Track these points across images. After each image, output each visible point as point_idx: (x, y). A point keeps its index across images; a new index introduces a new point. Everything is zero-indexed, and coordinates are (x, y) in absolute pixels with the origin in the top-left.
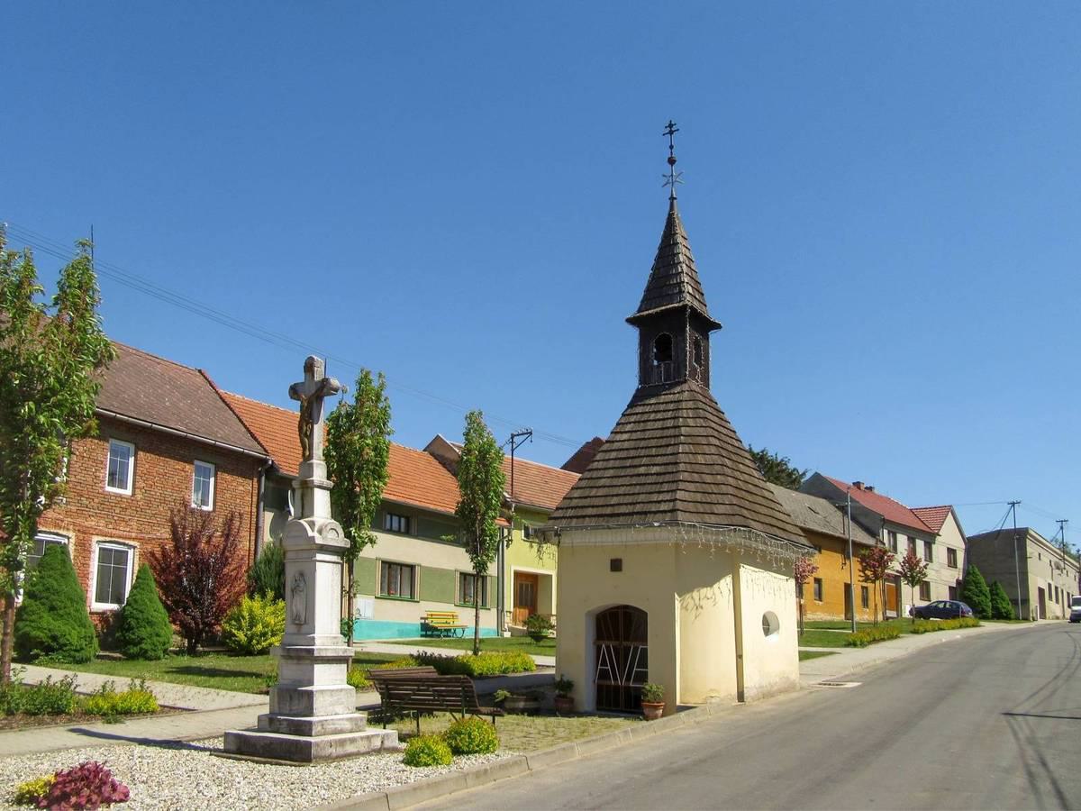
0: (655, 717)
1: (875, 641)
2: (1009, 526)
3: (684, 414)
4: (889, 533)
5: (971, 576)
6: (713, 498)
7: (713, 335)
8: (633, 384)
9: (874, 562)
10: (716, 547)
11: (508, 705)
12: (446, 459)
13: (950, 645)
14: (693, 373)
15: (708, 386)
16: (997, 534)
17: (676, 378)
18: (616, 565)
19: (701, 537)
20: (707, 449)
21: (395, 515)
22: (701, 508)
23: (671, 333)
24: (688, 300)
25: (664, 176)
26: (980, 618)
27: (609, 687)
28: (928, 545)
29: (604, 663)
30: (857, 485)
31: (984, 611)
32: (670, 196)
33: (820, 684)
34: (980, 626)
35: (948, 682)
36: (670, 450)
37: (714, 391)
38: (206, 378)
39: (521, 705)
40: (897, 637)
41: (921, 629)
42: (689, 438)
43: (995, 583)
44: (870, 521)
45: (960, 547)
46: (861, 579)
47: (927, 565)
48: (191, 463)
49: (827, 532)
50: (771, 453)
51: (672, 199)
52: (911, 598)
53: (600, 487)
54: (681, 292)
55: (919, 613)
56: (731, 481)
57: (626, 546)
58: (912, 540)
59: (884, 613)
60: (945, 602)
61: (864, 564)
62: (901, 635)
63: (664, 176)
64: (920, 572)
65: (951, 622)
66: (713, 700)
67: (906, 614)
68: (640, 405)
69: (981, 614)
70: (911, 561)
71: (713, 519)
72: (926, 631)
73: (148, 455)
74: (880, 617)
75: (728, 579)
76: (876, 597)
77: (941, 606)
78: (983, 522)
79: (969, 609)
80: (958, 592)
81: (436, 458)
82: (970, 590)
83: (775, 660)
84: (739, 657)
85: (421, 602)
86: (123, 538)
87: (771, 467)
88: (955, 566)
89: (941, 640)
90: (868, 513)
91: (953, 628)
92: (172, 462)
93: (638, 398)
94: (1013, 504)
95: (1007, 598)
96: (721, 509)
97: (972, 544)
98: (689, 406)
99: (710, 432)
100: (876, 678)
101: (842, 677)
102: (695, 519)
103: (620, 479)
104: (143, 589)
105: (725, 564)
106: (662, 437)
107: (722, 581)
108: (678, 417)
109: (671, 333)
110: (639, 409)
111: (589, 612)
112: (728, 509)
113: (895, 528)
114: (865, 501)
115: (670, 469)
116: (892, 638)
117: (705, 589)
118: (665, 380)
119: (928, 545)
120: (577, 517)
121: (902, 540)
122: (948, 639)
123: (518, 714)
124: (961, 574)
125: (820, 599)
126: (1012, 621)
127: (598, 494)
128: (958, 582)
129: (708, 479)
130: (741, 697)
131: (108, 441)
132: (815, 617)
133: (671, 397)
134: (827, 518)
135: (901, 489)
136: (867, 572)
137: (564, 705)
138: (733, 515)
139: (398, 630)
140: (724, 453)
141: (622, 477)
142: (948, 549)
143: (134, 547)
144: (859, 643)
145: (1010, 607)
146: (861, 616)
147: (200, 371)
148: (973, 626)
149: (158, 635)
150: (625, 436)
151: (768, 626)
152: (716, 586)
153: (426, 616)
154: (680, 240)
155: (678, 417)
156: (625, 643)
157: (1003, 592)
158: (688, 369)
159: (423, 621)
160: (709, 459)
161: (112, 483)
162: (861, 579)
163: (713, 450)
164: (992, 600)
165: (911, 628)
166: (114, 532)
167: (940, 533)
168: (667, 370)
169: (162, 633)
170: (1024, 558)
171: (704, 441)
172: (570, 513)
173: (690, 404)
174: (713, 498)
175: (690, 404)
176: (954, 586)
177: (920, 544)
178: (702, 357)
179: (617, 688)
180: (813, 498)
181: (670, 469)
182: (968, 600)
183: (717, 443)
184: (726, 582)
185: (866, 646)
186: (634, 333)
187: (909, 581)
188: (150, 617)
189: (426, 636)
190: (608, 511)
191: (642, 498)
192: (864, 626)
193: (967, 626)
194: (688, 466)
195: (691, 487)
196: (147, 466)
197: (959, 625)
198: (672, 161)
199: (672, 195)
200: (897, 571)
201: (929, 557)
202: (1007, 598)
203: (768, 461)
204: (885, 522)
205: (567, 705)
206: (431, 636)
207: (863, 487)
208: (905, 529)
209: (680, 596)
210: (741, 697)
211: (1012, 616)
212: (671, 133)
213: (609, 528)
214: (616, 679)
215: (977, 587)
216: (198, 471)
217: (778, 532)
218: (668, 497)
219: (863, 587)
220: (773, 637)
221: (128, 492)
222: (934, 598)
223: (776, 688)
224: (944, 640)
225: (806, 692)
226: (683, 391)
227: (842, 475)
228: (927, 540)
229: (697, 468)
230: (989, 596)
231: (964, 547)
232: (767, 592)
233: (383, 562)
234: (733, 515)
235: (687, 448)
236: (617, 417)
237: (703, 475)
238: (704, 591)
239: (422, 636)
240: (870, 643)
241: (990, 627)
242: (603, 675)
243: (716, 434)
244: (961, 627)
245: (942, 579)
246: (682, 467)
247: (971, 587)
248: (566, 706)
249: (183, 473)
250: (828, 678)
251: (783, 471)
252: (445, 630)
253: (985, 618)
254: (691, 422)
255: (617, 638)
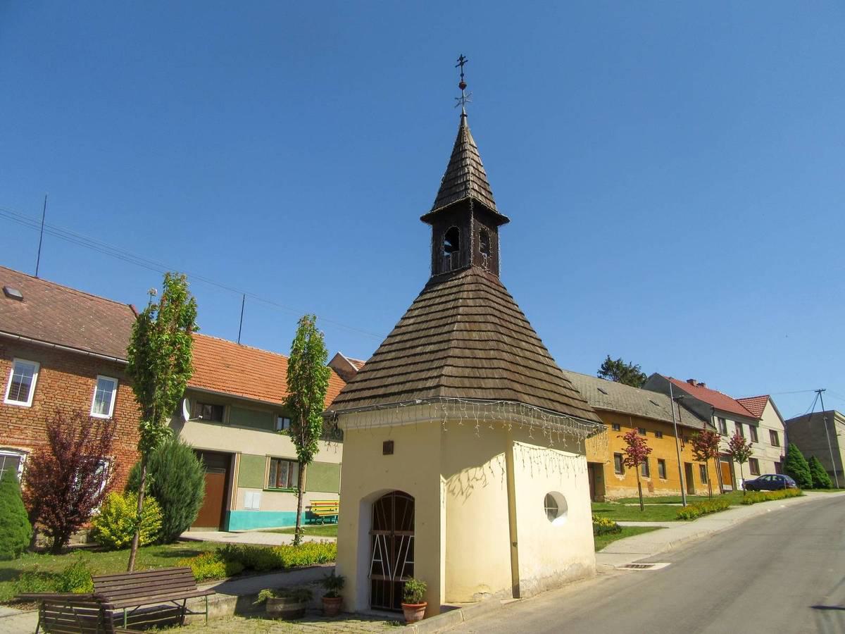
0: (416, 620)
1: (704, 513)
2: (818, 409)
3: (465, 295)
4: (719, 420)
5: (791, 453)
6: (483, 373)
7: (502, 229)
8: (427, 275)
9: (705, 444)
10: (481, 422)
11: (269, 608)
12: (343, 371)
13: (776, 514)
14: (479, 260)
15: (497, 273)
16: (810, 417)
17: (461, 265)
18: (388, 448)
19: (463, 413)
20: (483, 327)
21: (287, 418)
22: (467, 382)
23: (461, 225)
24: (472, 194)
25: (456, 98)
26: (803, 489)
27: (381, 581)
28: (753, 429)
29: (377, 556)
30: (691, 382)
31: (806, 482)
32: (461, 114)
33: (627, 566)
34: (729, 509)
35: (757, 562)
36: (446, 329)
37: (504, 277)
38: (134, 311)
39: (280, 607)
40: (727, 509)
41: (750, 500)
42: (465, 317)
43: (813, 458)
44: (704, 410)
45: (780, 429)
46: (695, 458)
47: (751, 444)
48: (94, 377)
49: (666, 420)
50: (626, 363)
51: (463, 115)
52: (743, 472)
53: (381, 369)
54: (467, 189)
55: (749, 486)
56: (505, 356)
57: (392, 427)
58: (739, 425)
59: (721, 487)
60: (772, 476)
61: (696, 445)
62: (731, 507)
63: (456, 98)
64: (746, 451)
65: (777, 493)
66: (483, 597)
67: (740, 488)
68: (429, 292)
69: (803, 485)
70: (738, 442)
71: (480, 394)
72: (754, 502)
73: (51, 371)
74: (716, 491)
75: (501, 458)
76: (713, 474)
77: (769, 479)
78: (797, 408)
79: (792, 481)
80: (783, 466)
81: (335, 372)
82: (792, 465)
83: (561, 546)
84: (514, 544)
85: (307, 492)
86: (16, 445)
87: (626, 373)
88: (778, 445)
89: (766, 510)
90: (700, 403)
91: (779, 499)
92: (74, 377)
93: (430, 286)
94: (820, 391)
95: (824, 470)
96: (490, 383)
97: (790, 426)
98: (470, 289)
99: (490, 311)
100: (683, 558)
101: (658, 555)
102: (458, 394)
103: (399, 360)
104: (5, 491)
105: (497, 441)
106: (442, 318)
107: (494, 460)
108: (459, 299)
109: (461, 225)
110: (428, 296)
111: (363, 498)
112: (498, 383)
113: (724, 415)
114: (695, 393)
115: (443, 346)
116: (721, 509)
117: (474, 469)
118: (453, 268)
119: (753, 429)
120: (354, 400)
121: (731, 425)
122: (773, 509)
123: (276, 619)
124: (784, 451)
125: (665, 478)
126: (831, 490)
127: (377, 376)
128: (782, 458)
129: (480, 354)
130: (516, 592)
131: (12, 361)
132: (662, 493)
133: (456, 282)
134: (660, 407)
135: (727, 384)
136: (699, 452)
137: (330, 606)
138: (502, 389)
139: (284, 519)
140: (502, 330)
141: (402, 357)
142: (770, 430)
143: (27, 453)
144: (688, 516)
145: (827, 478)
146: (701, 490)
147: (130, 306)
148: (797, 496)
149: (11, 535)
150: (412, 321)
151: (553, 506)
152: (486, 466)
153: (310, 505)
154: (468, 147)
155: (459, 299)
156: (397, 533)
157: (820, 466)
158: (472, 256)
159: (308, 510)
160: (484, 336)
161: (12, 397)
162: (695, 458)
163: (490, 327)
164: (812, 472)
165: (741, 500)
166: (7, 439)
167: (762, 418)
168: (455, 258)
169: (16, 532)
170: (834, 436)
171: (481, 319)
172: (350, 396)
173: (473, 287)
174: (483, 373)
175: (473, 287)
176: (779, 461)
177: (746, 428)
178: (490, 248)
179: (388, 582)
180: (654, 393)
181: (443, 346)
182: (791, 473)
183: (497, 321)
184: (498, 462)
185: (696, 518)
186: (428, 230)
187: (738, 459)
188: (5, 519)
189: (310, 523)
190: (381, 391)
191: (412, 376)
192: (702, 499)
193: (792, 496)
194: (461, 342)
195: (461, 362)
196: (49, 381)
197: (784, 496)
198: (462, 86)
199: (463, 113)
200: (727, 451)
201: (755, 438)
202: (824, 470)
203: (623, 369)
204: (715, 411)
205: (334, 606)
206: (315, 523)
207: (695, 384)
208: (732, 415)
209: (446, 478)
210: (516, 592)
211: (831, 485)
212: (462, 64)
213: (378, 409)
214: (387, 574)
215: (797, 462)
216: (102, 385)
217: (558, 407)
218: (435, 373)
219: (700, 465)
220: (560, 520)
221: (28, 404)
222: (762, 473)
223: (564, 577)
224: (769, 510)
225: (673, 554)
226: (466, 276)
227: (678, 373)
228: (752, 424)
229: (471, 344)
230: (809, 469)
231: (783, 429)
232: (549, 470)
233: (272, 458)
234: (502, 389)
235: (462, 326)
236: (409, 304)
237: (475, 351)
238: (472, 472)
239: (306, 523)
240: (699, 516)
241: (811, 496)
242: (376, 569)
243: (497, 313)
244: (786, 497)
245: (768, 456)
246: (454, 343)
247: (793, 462)
248: (332, 606)
249: (85, 387)
250: (641, 558)
251: (635, 376)
252: (326, 517)
253: (808, 488)
254: (470, 302)
255: (389, 529)
